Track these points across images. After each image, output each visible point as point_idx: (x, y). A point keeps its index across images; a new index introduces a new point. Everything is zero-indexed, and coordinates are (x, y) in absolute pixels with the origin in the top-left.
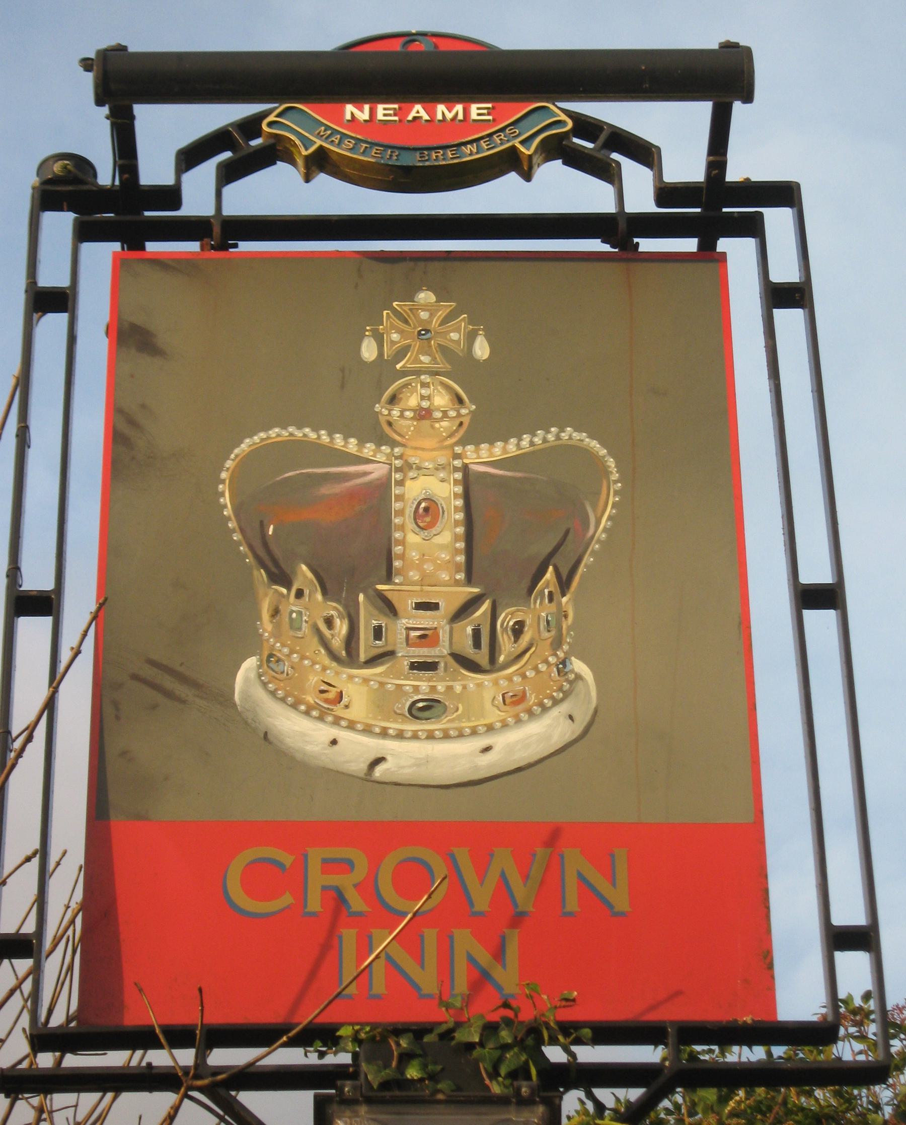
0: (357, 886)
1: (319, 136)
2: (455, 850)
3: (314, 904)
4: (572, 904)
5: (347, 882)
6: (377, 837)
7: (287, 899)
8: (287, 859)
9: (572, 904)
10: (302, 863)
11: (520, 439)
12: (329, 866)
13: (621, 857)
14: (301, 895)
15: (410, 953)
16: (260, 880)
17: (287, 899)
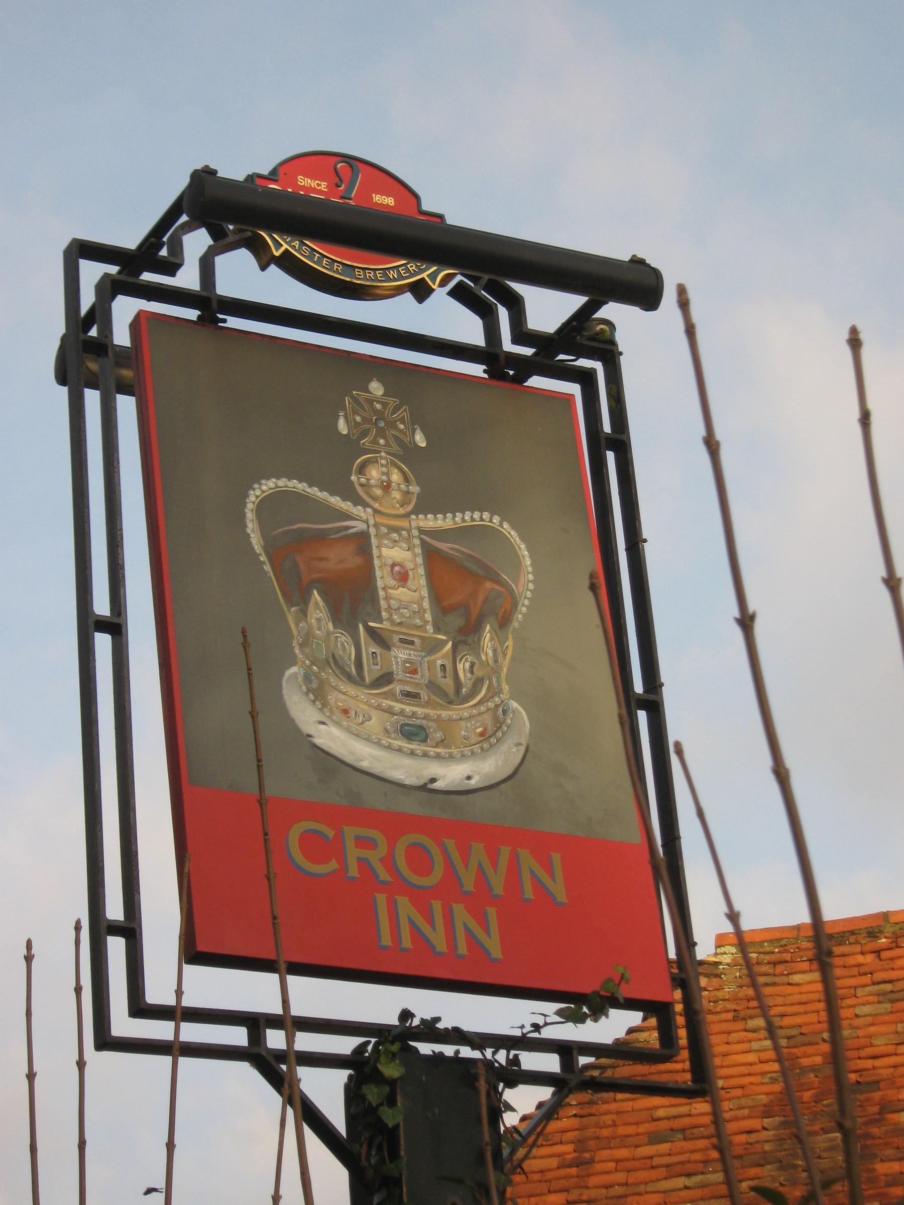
0: (381, 860)
1: (286, 243)
2: (389, 879)
3: (353, 871)
4: (529, 894)
5: (374, 857)
6: (394, 824)
7: (333, 865)
8: (331, 833)
9: (529, 894)
10: (339, 836)
11: (454, 516)
12: (361, 843)
13: (556, 858)
14: (342, 861)
15: (423, 915)
16: (314, 846)
17: (333, 865)
